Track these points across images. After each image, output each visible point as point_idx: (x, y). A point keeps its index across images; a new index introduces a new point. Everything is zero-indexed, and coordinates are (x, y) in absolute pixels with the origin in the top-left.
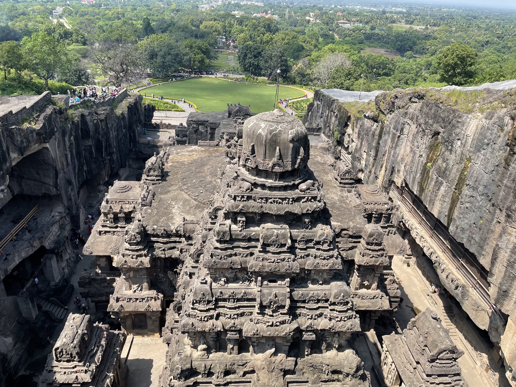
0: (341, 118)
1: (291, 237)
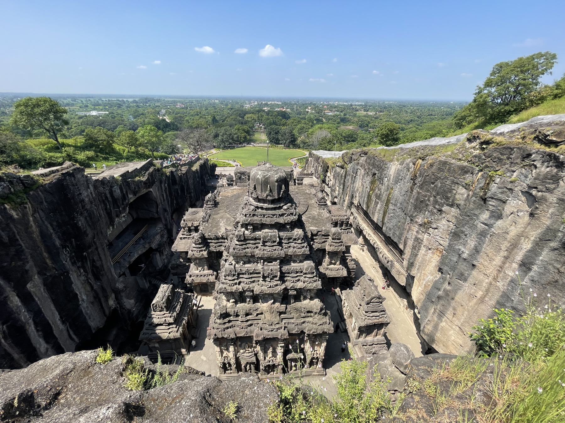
0: (324, 167)
1: (279, 237)
